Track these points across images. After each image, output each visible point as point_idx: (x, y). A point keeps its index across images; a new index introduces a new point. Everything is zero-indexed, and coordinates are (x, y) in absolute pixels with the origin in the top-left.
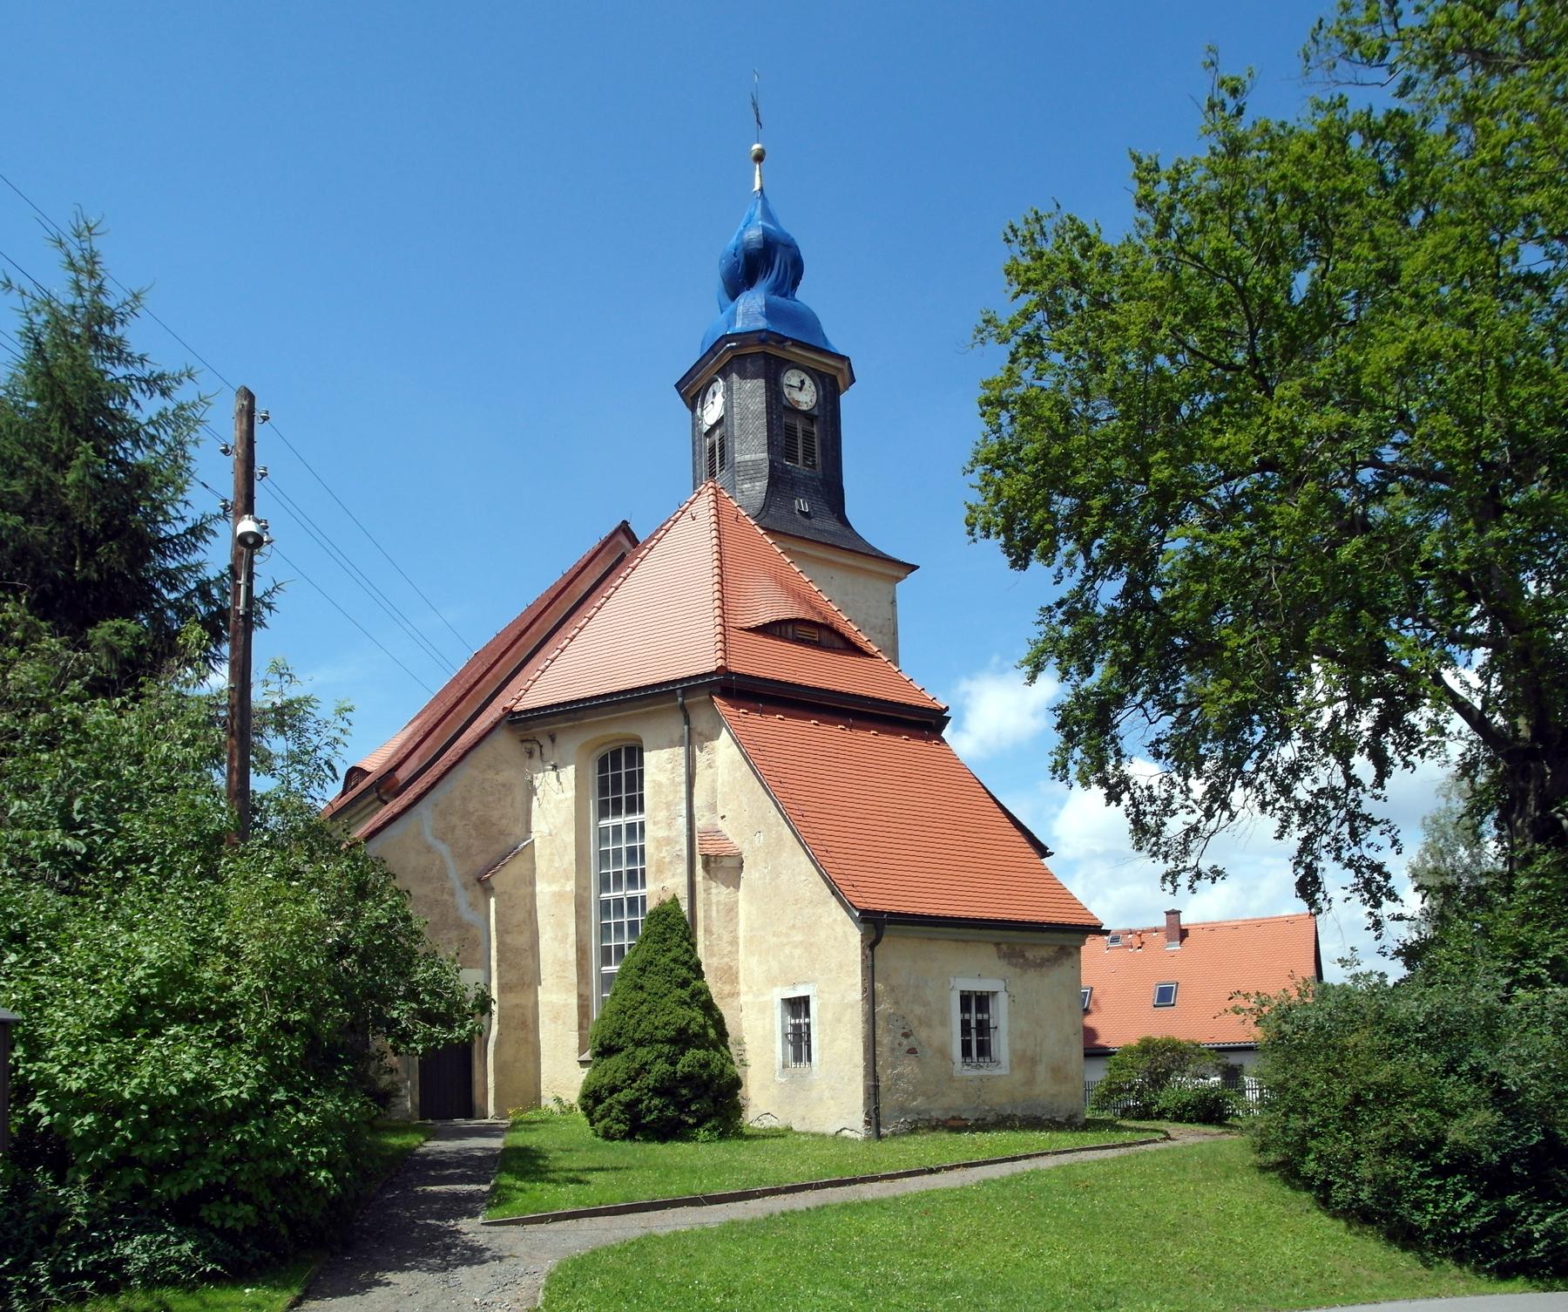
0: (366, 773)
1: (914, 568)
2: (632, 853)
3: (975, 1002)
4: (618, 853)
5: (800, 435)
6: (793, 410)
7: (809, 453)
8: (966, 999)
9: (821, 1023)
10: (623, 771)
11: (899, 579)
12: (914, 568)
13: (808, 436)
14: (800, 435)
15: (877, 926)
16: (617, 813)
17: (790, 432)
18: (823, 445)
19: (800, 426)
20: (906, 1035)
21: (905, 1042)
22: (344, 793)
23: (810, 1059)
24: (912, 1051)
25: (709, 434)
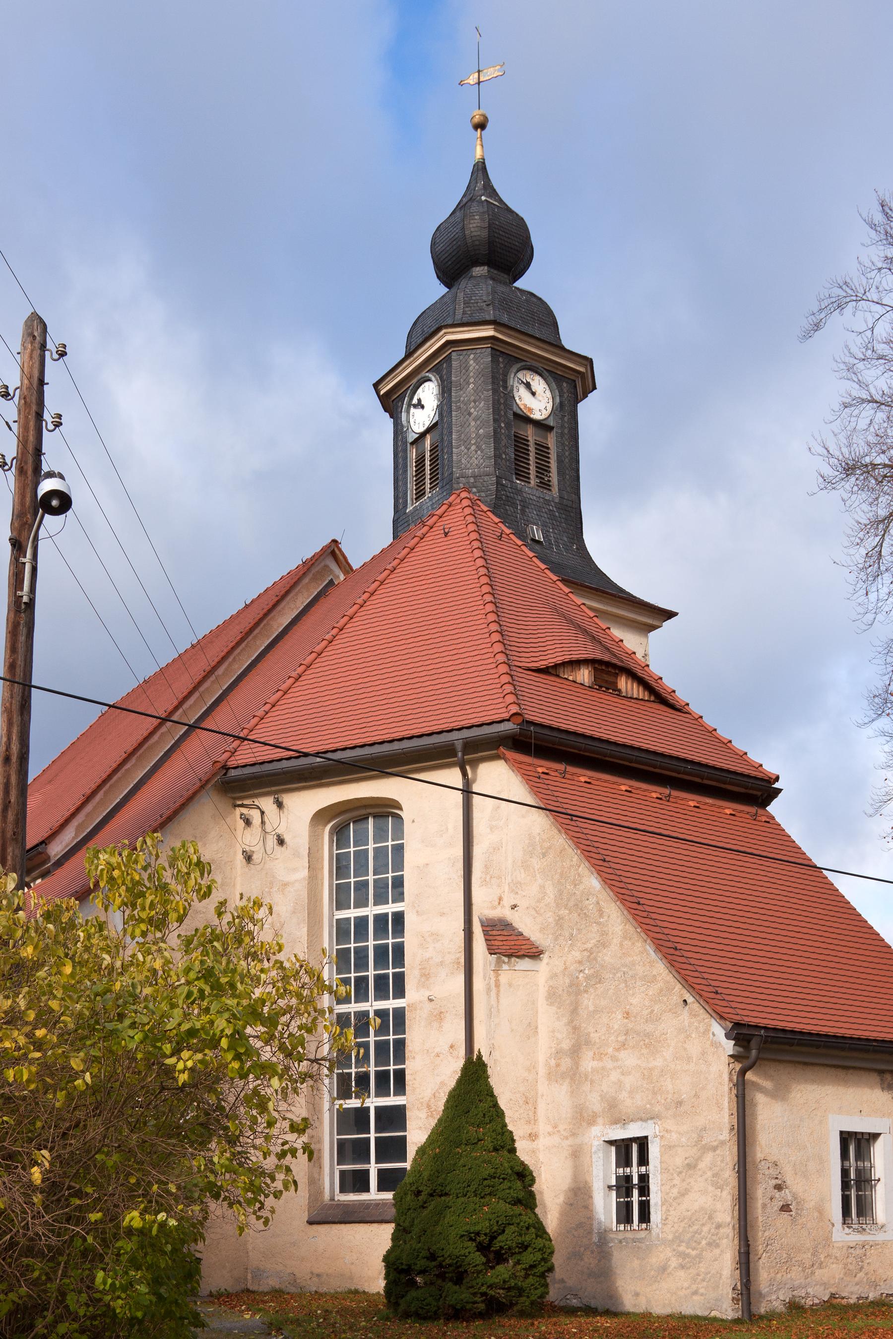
0: (531, 413)
1: (669, 615)
2: (381, 953)
3: (855, 1144)
4: (361, 954)
5: (532, 448)
6: (524, 419)
7: (543, 470)
8: (846, 1138)
9: (665, 1170)
10: (371, 846)
11: (654, 628)
12: (669, 615)
13: (542, 450)
14: (532, 448)
15: (742, 1034)
16: (362, 902)
17: (520, 444)
18: (560, 461)
19: (530, 434)
20: (779, 1187)
21: (777, 1194)
22: (76, 835)
23: (645, 1216)
24: (786, 1208)
25: (28, 851)
